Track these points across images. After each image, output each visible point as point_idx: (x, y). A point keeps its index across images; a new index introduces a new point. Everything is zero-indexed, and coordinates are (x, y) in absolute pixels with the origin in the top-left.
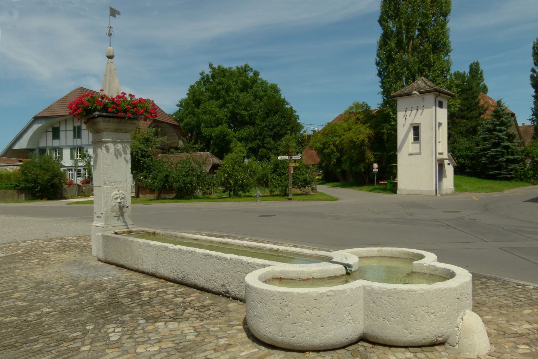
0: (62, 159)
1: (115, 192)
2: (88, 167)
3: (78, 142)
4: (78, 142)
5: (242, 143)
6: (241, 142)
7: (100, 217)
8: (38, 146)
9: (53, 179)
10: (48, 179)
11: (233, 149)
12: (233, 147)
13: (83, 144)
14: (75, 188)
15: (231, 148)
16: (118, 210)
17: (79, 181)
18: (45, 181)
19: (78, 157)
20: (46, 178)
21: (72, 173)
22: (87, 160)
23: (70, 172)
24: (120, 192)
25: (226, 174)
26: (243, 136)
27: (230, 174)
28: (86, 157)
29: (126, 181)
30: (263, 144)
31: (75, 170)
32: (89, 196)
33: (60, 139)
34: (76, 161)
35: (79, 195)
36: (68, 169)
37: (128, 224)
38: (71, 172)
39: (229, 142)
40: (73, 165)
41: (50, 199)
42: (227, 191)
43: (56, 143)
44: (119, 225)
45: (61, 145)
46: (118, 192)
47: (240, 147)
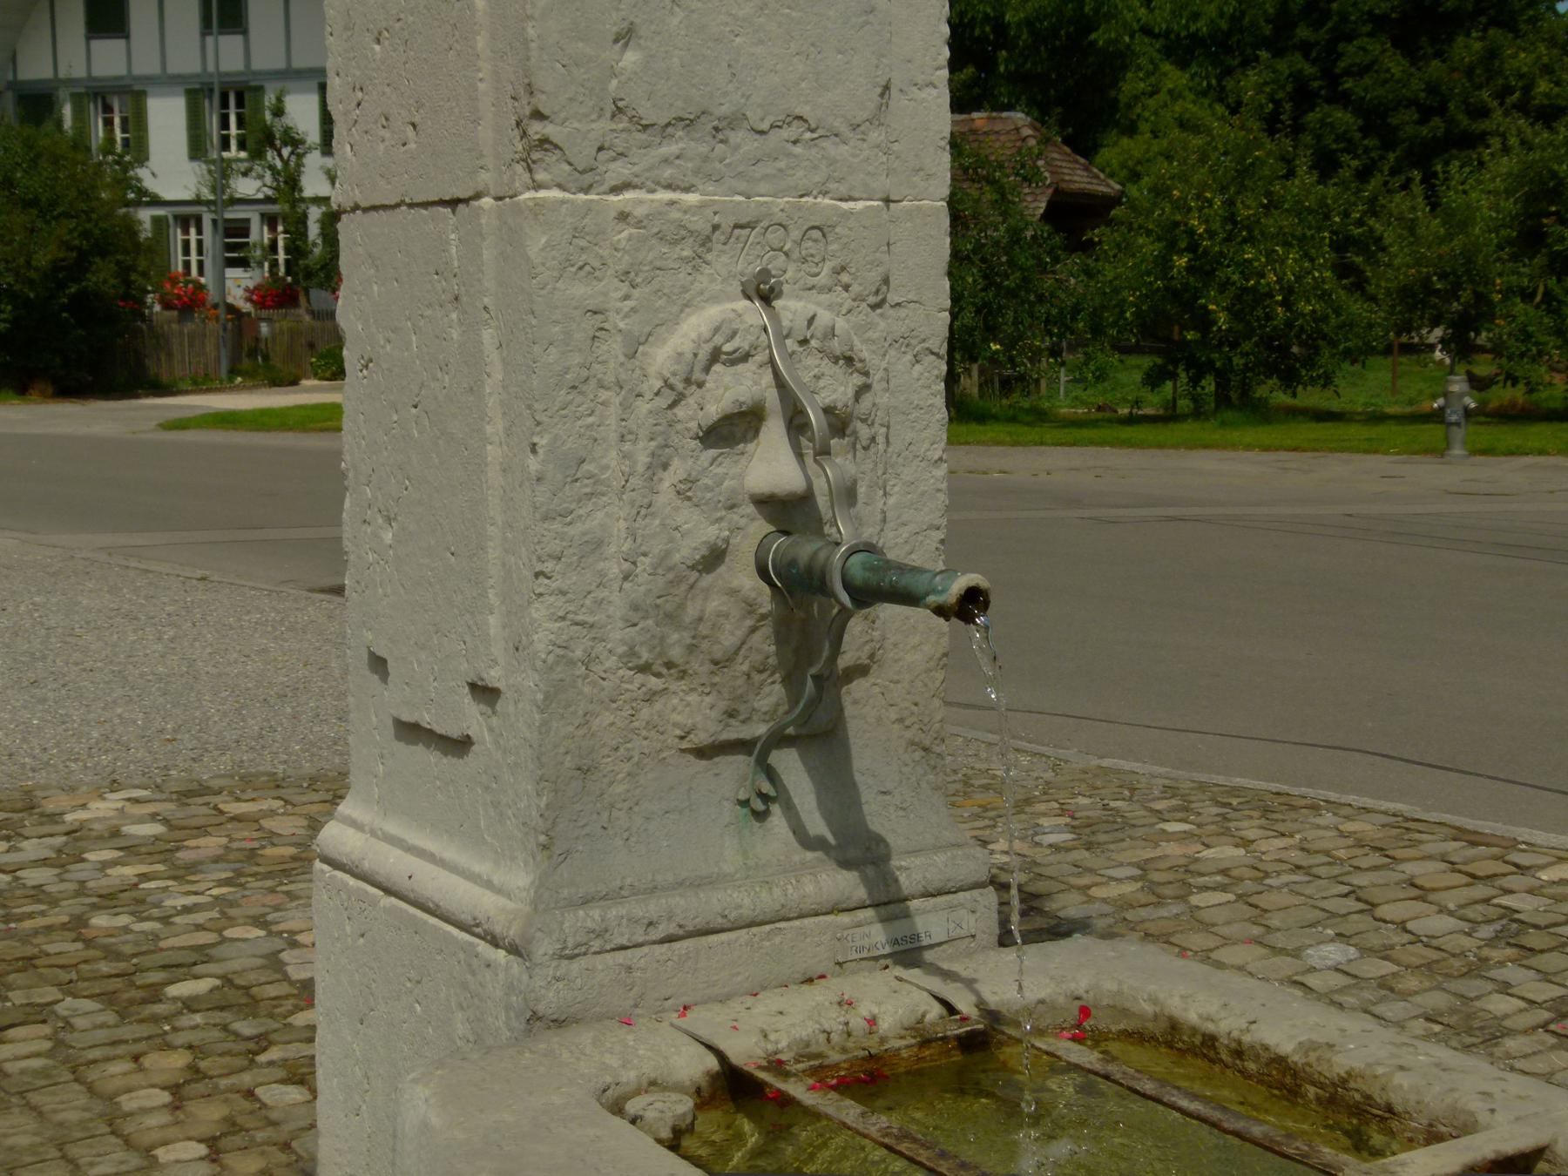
0: (142, 157)
1: (714, 313)
2: (286, 207)
3: (229, 55)
4: (229, 55)
5: (1194, 68)
6: (1183, 65)
7: (460, 745)
8: (10, 77)
9: (81, 265)
10: (56, 266)
11: (1138, 110)
12: (1136, 98)
13: (257, 65)
14: (212, 325)
15: (1123, 99)
16: (764, 644)
17: (238, 285)
18: (33, 275)
19: (233, 144)
20: (43, 259)
21: (200, 243)
22: (279, 164)
23: (186, 232)
24: (792, 307)
25: (1180, 253)
26: (1202, 26)
27: (1206, 252)
28: (273, 146)
29: (876, 120)
30: (1332, 79)
31: (214, 222)
32: (294, 382)
33: (127, 37)
34: (224, 172)
35: (239, 373)
36: (176, 217)
37: (910, 872)
38: (193, 236)
39: (1116, 62)
40: (207, 195)
41: (68, 389)
42: (1173, 376)
43: (109, 59)
44: (768, 900)
45: (138, 70)
46: (754, 312)
47: (1180, 96)
